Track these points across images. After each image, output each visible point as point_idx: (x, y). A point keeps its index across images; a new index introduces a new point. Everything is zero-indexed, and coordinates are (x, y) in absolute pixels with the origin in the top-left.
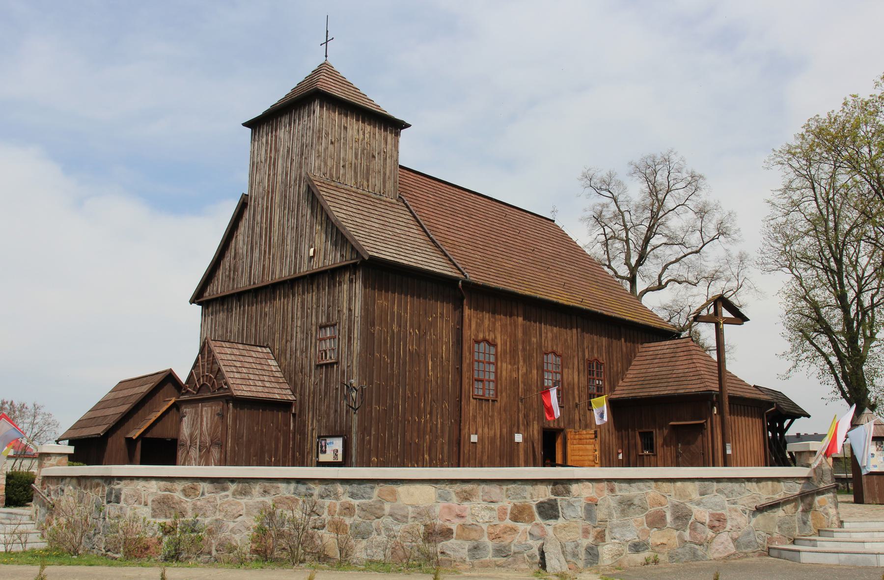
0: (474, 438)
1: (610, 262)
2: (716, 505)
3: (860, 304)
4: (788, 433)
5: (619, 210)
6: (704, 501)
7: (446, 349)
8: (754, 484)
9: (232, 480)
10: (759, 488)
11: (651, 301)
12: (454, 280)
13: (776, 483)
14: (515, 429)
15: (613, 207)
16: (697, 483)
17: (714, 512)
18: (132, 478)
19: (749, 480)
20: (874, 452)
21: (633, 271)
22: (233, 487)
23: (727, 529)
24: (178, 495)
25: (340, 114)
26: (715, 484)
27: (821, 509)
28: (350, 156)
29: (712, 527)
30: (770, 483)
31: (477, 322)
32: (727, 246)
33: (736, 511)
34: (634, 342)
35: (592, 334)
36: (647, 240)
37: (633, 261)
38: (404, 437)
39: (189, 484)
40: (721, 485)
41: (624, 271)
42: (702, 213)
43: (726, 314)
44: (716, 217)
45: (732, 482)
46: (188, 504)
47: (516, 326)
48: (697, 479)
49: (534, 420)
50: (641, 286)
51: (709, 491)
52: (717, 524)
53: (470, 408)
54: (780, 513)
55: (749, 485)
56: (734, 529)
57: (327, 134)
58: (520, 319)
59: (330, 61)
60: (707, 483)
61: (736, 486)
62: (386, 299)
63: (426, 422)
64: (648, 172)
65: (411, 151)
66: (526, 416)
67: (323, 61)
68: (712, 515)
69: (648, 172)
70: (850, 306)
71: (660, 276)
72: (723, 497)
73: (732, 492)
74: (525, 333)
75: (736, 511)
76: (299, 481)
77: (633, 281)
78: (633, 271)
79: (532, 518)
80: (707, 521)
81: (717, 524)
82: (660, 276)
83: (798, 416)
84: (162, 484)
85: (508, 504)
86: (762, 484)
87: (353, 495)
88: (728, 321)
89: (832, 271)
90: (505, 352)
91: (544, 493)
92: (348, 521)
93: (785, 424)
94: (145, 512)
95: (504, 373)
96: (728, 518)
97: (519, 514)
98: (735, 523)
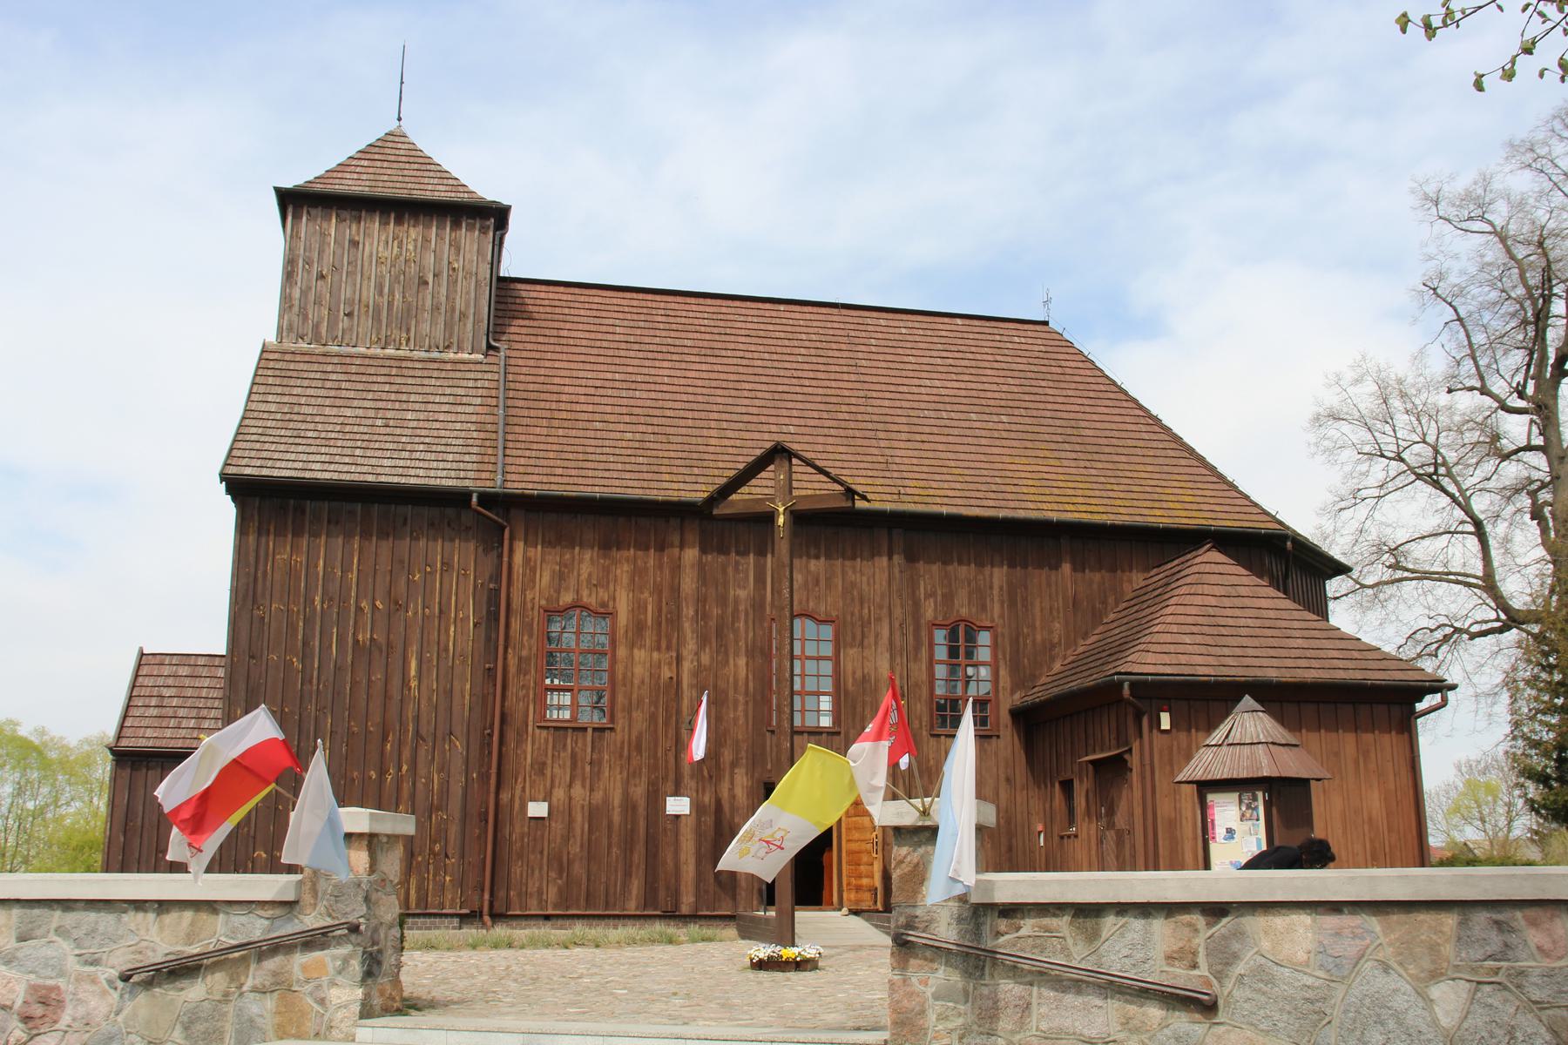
0: (538, 809)
1: (1482, 378)
2: (46, 965)
5: (1512, 257)
6: (19, 954)
7: (462, 632)
8: (151, 916)
10: (161, 929)
13: (204, 916)
14: (670, 786)
16: (16, 912)
17: (40, 981)
19: (139, 905)
20: (1234, 824)
23: (61, 1025)
25: (340, 220)
26: (58, 913)
27: (309, 987)
28: (370, 294)
29: (27, 1019)
30: (188, 915)
31: (534, 568)
33: (94, 981)
34: (1113, 570)
35: (945, 563)
40: (70, 918)
45: (99, 910)
47: (677, 568)
48: (18, 901)
49: (734, 765)
51: (38, 932)
52: (38, 1010)
54: (195, 991)
55: (132, 919)
56: (76, 1025)
57: (308, 262)
58: (691, 554)
59: (407, 127)
60: (36, 912)
61: (106, 920)
62: (295, 549)
63: (399, 781)
65: (522, 256)
67: (392, 125)
68: (34, 988)
72: (65, 946)
73: (92, 933)
75: (94, 981)
80: (19, 1003)
81: (38, 1010)
86: (170, 918)
90: (638, 627)
95: (638, 670)
96: (68, 998)
98: (81, 1010)
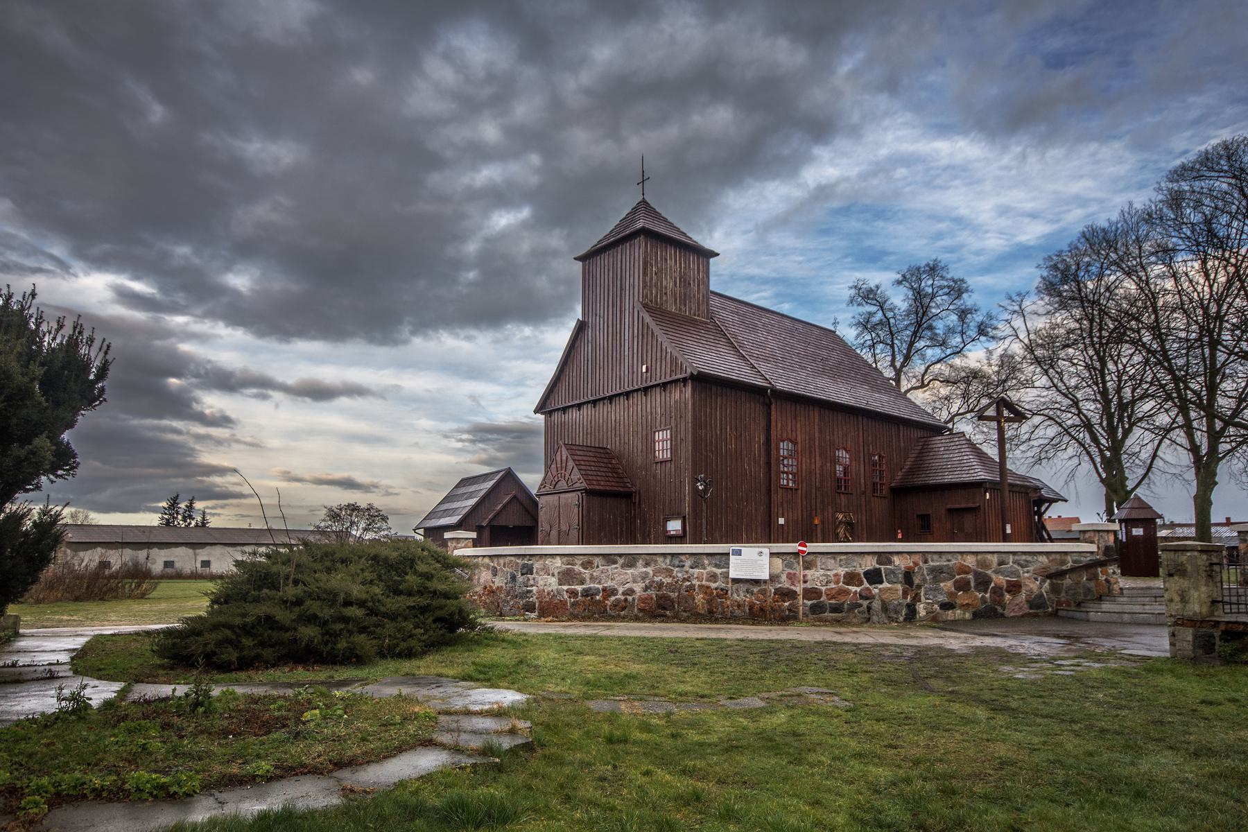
0: (781, 521)
3: (1120, 398)
4: (1046, 516)
9: (620, 555)
11: (919, 397)
12: (764, 389)
15: (879, 315)
18: (541, 556)
21: (898, 372)
22: (621, 561)
24: (578, 568)
32: (986, 345)
36: (911, 344)
37: (898, 364)
38: (726, 520)
39: (586, 559)
41: (889, 373)
42: (963, 314)
43: (1006, 413)
44: (979, 318)
46: (586, 573)
50: (905, 385)
53: (777, 497)
64: (913, 277)
66: (822, 502)
69: (913, 277)
70: (1111, 401)
71: (923, 376)
74: (820, 432)
76: (673, 555)
77: (898, 380)
78: (898, 372)
79: (861, 584)
82: (923, 376)
83: (1056, 501)
84: (565, 559)
85: (842, 571)
87: (717, 566)
88: (1008, 420)
89: (1095, 369)
91: (870, 563)
92: (713, 585)
93: (1043, 509)
94: (553, 581)
97: (851, 578)
